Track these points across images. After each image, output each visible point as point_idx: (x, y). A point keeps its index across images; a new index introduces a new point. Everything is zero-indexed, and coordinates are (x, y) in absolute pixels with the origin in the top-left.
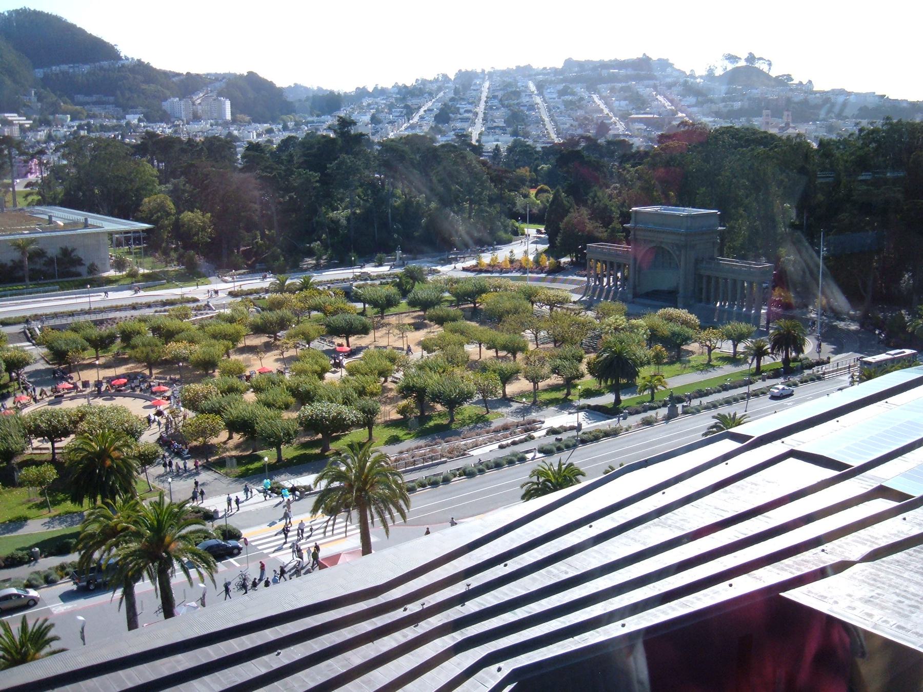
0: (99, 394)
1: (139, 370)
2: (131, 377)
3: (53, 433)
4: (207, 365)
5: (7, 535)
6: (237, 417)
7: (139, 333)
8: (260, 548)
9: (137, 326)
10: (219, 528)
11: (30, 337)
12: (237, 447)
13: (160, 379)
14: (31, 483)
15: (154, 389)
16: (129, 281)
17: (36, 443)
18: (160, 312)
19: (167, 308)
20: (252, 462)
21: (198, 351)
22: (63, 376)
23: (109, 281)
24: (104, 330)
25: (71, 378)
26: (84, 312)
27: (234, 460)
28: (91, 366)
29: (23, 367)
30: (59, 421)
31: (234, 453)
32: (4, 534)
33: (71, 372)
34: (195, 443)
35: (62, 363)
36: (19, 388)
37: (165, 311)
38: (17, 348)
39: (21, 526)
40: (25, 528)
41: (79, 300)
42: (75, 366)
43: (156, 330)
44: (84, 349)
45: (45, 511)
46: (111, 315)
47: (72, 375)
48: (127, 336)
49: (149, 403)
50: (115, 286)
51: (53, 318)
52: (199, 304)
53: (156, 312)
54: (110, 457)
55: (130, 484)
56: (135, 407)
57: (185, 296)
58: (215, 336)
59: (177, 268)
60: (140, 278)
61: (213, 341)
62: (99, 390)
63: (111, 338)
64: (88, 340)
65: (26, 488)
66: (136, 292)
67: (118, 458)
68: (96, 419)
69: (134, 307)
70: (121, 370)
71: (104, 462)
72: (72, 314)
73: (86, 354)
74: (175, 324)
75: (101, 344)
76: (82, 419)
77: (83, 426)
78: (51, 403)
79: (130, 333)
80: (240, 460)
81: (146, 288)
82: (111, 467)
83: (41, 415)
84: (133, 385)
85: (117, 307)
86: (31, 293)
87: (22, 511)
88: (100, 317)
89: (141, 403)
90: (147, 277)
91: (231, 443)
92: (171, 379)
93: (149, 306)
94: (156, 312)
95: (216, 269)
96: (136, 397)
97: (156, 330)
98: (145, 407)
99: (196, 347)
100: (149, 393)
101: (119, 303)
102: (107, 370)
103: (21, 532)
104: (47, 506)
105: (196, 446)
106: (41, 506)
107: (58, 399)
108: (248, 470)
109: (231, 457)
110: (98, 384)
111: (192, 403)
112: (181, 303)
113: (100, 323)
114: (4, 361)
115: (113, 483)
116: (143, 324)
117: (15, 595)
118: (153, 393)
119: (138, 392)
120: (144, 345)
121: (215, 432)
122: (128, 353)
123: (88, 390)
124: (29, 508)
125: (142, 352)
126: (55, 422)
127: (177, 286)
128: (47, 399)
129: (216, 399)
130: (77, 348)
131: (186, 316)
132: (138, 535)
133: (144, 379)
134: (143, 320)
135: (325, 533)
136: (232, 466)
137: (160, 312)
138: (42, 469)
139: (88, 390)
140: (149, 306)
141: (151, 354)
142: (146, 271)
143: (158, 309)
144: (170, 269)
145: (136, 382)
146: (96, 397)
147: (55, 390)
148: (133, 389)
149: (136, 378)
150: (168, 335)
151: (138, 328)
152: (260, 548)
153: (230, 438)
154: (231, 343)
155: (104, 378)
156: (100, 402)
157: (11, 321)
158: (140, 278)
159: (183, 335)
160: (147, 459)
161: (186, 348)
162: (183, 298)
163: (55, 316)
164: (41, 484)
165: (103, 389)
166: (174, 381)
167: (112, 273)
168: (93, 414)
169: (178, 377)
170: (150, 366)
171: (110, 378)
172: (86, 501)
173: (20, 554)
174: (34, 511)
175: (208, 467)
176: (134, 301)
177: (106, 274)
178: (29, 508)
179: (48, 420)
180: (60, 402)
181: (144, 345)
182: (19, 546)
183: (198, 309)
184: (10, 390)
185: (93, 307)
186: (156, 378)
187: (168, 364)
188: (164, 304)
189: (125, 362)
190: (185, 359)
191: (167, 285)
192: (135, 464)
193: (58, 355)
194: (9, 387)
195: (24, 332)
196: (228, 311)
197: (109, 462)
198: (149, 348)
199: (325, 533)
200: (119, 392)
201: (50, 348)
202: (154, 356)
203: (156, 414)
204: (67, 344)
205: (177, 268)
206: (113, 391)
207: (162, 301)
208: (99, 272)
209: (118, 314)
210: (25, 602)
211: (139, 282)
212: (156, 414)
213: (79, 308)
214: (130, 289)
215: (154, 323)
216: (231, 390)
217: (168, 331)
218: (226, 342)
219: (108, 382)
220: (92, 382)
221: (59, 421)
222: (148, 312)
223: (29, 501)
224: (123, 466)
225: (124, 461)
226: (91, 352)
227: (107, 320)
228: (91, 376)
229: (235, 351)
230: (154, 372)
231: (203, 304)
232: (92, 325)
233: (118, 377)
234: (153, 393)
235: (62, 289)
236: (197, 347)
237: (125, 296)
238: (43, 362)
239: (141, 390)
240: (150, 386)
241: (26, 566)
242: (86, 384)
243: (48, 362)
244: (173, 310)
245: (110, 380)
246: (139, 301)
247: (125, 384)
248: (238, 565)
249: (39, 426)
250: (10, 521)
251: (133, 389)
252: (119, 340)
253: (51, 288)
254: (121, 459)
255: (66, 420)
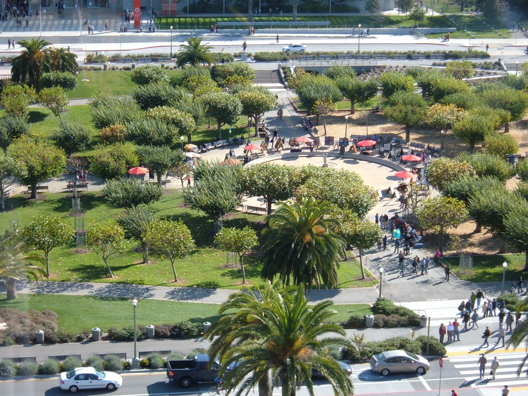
0: (341, 154)
1: (396, 132)
2: (381, 139)
3: (273, 192)
4: (473, 137)
5: (189, 301)
6: (486, 207)
7: (404, 88)
8: (462, 373)
9: (402, 78)
10: (420, 339)
11: (282, 77)
12: (482, 243)
13: (417, 146)
14: (228, 247)
15: (404, 157)
16: (412, 23)
17: (254, 201)
18: (440, 65)
19: (449, 61)
20: (492, 266)
21: (466, 118)
22: (308, 127)
23: (389, 22)
24: (366, 80)
25: (316, 131)
26: (350, 56)
27: (470, 259)
28: (341, 120)
29: (263, 111)
30: (278, 180)
31: (476, 250)
32: (187, 299)
33: (317, 124)
34: (431, 231)
35: (311, 110)
36: (256, 135)
37: (445, 65)
38: (260, 89)
39: (208, 294)
40: (212, 297)
41: (349, 41)
42: (323, 118)
43: (426, 87)
44: (335, 100)
45: (239, 281)
46: (380, 63)
47: (317, 127)
48: (389, 90)
49: (394, 173)
50: (394, 28)
51: (314, 58)
52: (488, 61)
53: (434, 65)
54: (310, 231)
55: (329, 266)
56: (372, 176)
57: (474, 49)
58: (494, 104)
59: (474, 14)
60: (425, 21)
61: (488, 109)
62: (342, 150)
63: (371, 90)
64: (343, 89)
65: (220, 251)
66: (447, 38)
67: (320, 234)
68: (318, 183)
69: (409, 56)
70: (375, 130)
71: (303, 235)
72: (336, 56)
73: (336, 106)
74: (451, 82)
75: (358, 95)
76: (303, 181)
77: (303, 189)
78: (285, 158)
79: (394, 86)
80: (477, 259)
81: (428, 34)
82: (310, 243)
83: (260, 171)
84: (382, 149)
85: (390, 53)
86: (296, 27)
87: (215, 276)
88: (366, 63)
89: (387, 171)
90: (435, 22)
91: (477, 238)
92: (429, 148)
93: (427, 56)
94: (434, 65)
95: (521, 20)
96: (383, 164)
97: (426, 87)
98: (389, 178)
99: (466, 114)
100: (398, 161)
101: (393, 49)
102: (359, 128)
103: (206, 300)
104: (242, 276)
105: (433, 234)
106: (236, 274)
107: (295, 153)
108: (485, 273)
109: (467, 254)
110: (344, 142)
111: (437, 180)
112: (467, 57)
113: (360, 71)
114: (243, 102)
115: (310, 262)
116: (410, 78)
117: (404, 358)
118: (404, 162)
119: (386, 159)
120: (405, 104)
121: (455, 221)
122: (388, 109)
123: (331, 148)
124: (223, 275)
125: (401, 111)
126: (273, 181)
127: (468, 36)
128: (283, 152)
129: (465, 181)
130: (327, 97)
131: (466, 74)
132: (264, 329)
133: (399, 143)
134: (414, 74)
135: (519, 372)
136: (467, 266)
137: (440, 65)
138: (244, 232)
139: (331, 148)
140: (427, 56)
141: (410, 115)
142: (436, 14)
143: (438, 61)
144: (465, 14)
145: (387, 146)
146: (337, 157)
147: (294, 143)
148: (381, 154)
149: (389, 141)
150: (435, 93)
151: (403, 82)
152: (462, 373)
153: (478, 231)
154: (509, 113)
155: (352, 136)
156: (339, 165)
157: (266, 57)
158: (425, 21)
159: (455, 96)
160: (361, 241)
161: (452, 113)
162: (470, 52)
163: (317, 56)
164: (238, 249)
165: (347, 149)
166: (433, 152)
167: (394, 13)
168: (317, 177)
169: (438, 146)
170: (409, 129)
171: (359, 137)
172: (277, 278)
173: (190, 325)
174: (228, 279)
175: (437, 261)
176: (412, 49)
177: (386, 13)
178: (223, 275)
179: (266, 177)
180: (295, 158)
181: (405, 104)
182: (194, 316)
183: (486, 67)
184: (246, 136)
185: (362, 51)
186: (412, 145)
187: (432, 129)
188: (447, 56)
189: (383, 119)
190: (449, 126)
191: (457, 34)
192: (339, 243)
193: (307, 103)
194: (245, 132)
195: (278, 71)
196: (519, 74)
197: (308, 237)
198: (410, 108)
199: (519, 372)
200: (365, 156)
201: (300, 94)
202: (413, 118)
203: (398, 189)
204: (318, 92)
205: (474, 14)
206: (358, 153)
207: (444, 53)
208: (378, 8)
209: (388, 63)
210: (414, 368)
211: (424, 26)
212: (398, 189)
213: (345, 50)
214: (411, 33)
215: (423, 78)
216: (491, 172)
217: (439, 90)
218: (503, 112)
219: (355, 142)
220: (337, 140)
221: (278, 180)
222: (425, 64)
223: (227, 267)
224: (323, 243)
225: (326, 238)
226: (346, 103)
227: (374, 67)
228: (337, 131)
229: (517, 125)
230: (412, 136)
231: (493, 61)
232: (353, 72)
233: (369, 138)
234: (404, 162)
235: (333, 25)
236: (467, 113)
237: (406, 42)
238: (290, 108)
239: (390, 157)
240: (402, 153)
241: (193, 340)
242: (329, 141)
243: (295, 110)
244: (451, 65)
245: (357, 139)
246: (418, 49)
247: (374, 147)
248: (428, 388)
249: (255, 183)
250: (198, 286)
251: (381, 154)
252: (379, 94)
253: (322, 23)
254: (325, 237)
255: (287, 179)
